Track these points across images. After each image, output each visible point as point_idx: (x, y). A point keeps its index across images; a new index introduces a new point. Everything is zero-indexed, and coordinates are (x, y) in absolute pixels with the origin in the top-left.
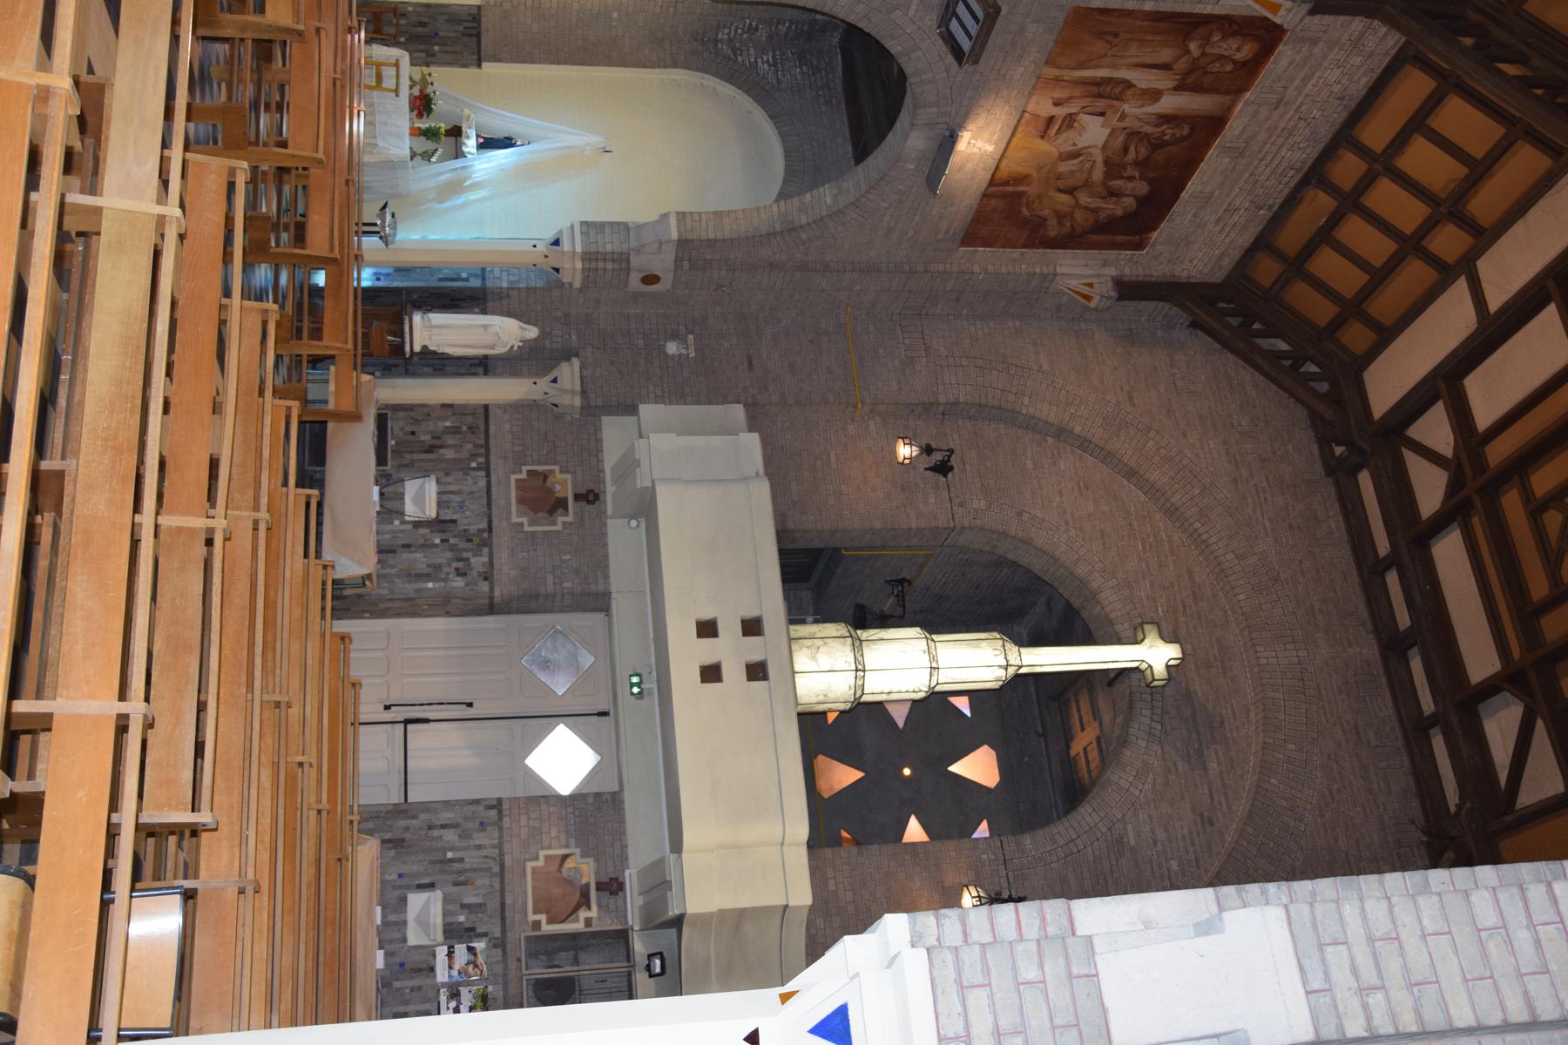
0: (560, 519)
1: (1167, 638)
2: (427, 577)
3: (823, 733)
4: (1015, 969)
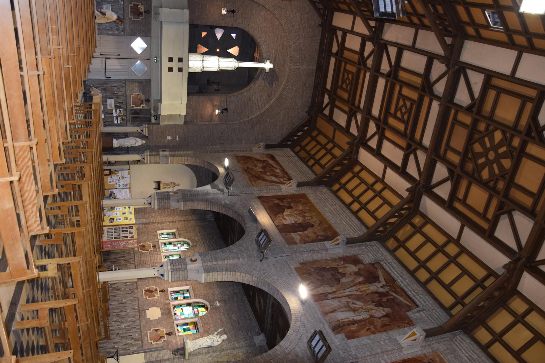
0: (141, 18)
2: (109, 30)
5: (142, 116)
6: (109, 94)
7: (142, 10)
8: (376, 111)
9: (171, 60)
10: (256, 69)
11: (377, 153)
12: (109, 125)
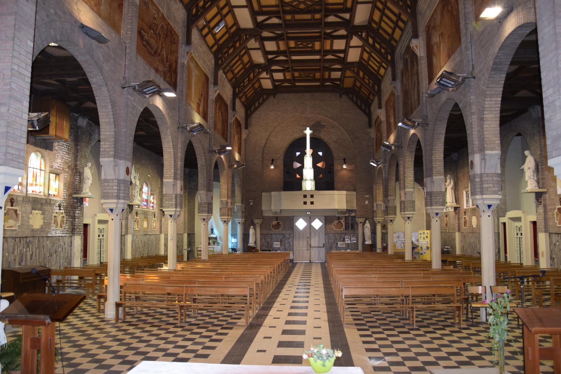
3: (319, 187)
6: (334, 246)
7: (276, 222)
9: (305, 203)
10: (311, 138)
12: (357, 246)
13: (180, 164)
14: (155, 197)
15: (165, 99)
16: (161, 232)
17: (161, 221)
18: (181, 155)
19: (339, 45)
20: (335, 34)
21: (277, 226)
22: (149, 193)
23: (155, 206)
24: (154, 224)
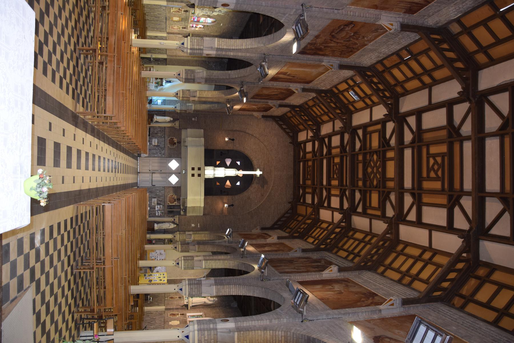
1: (260, 171)
4: (163, 284)
5: (175, 210)
7: (176, 142)
8: (408, 183)
9: (193, 169)
11: (419, 223)
12: (152, 217)
13: (231, 55)
14: (201, 29)
15: (291, 43)
16: (168, 33)
17: (179, 34)
18: (240, 55)
19: (335, 202)
20: (345, 198)
21: (172, 143)
22: (205, 24)
23: (193, 29)
24: (176, 27)
